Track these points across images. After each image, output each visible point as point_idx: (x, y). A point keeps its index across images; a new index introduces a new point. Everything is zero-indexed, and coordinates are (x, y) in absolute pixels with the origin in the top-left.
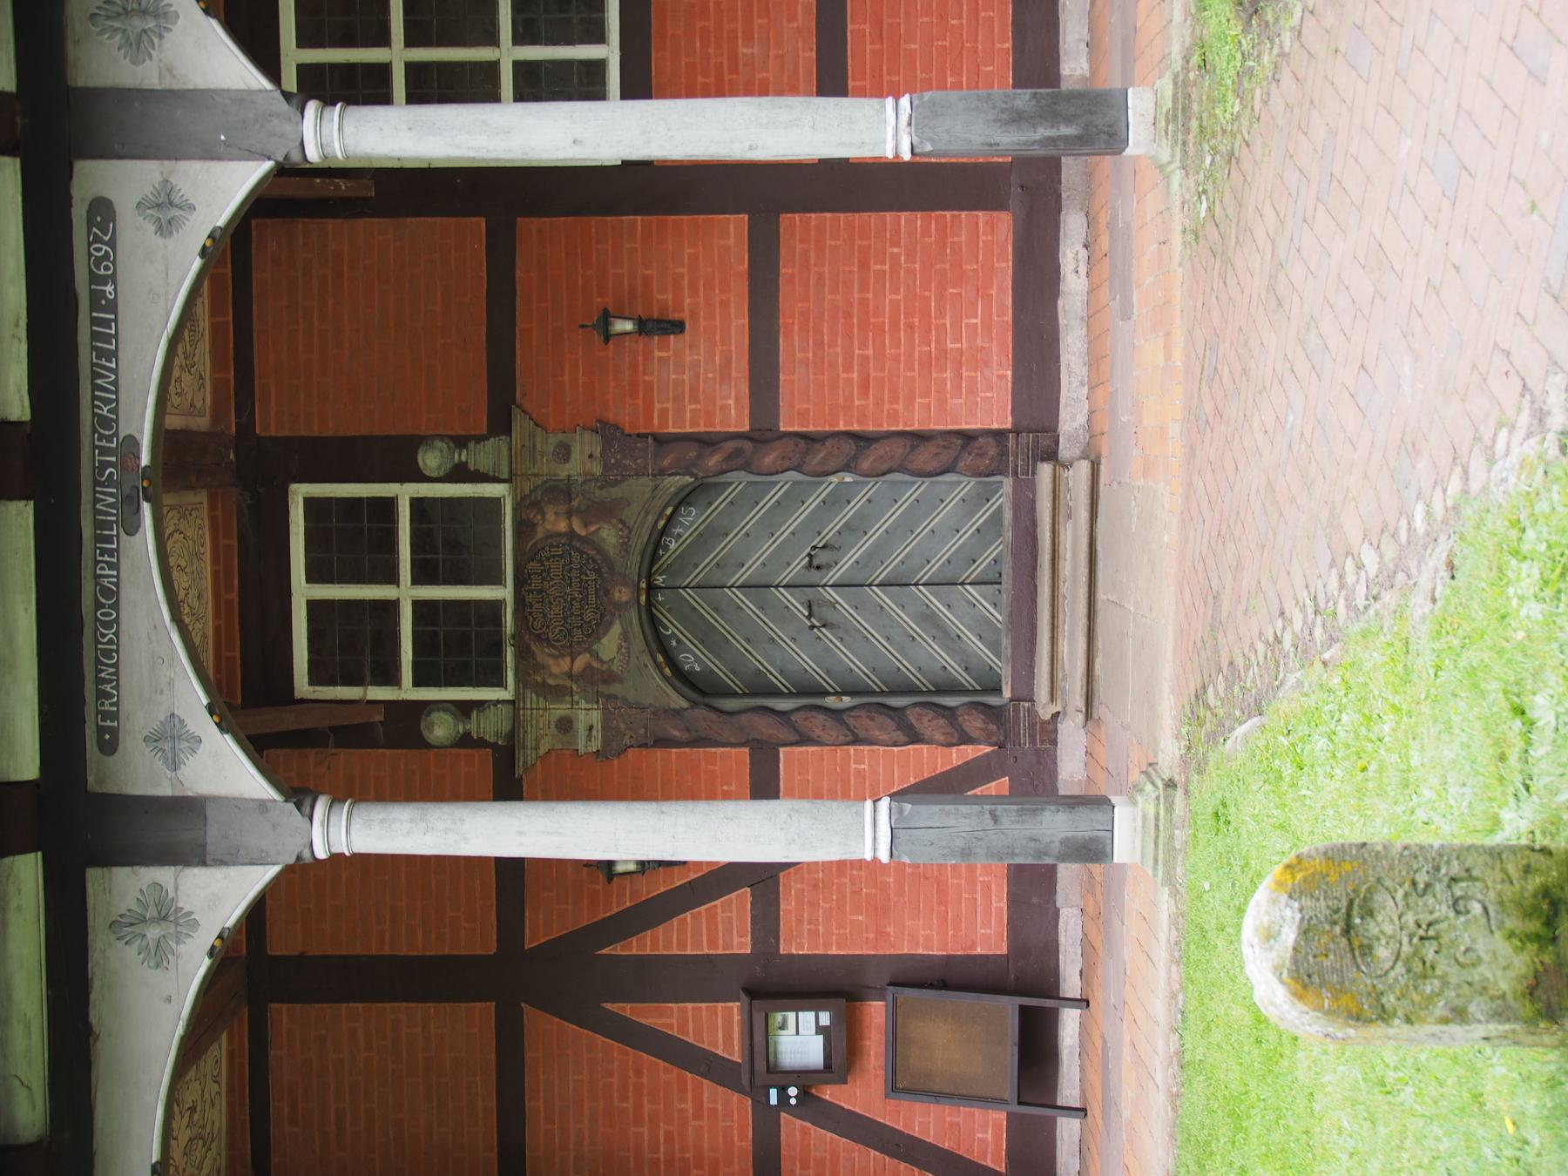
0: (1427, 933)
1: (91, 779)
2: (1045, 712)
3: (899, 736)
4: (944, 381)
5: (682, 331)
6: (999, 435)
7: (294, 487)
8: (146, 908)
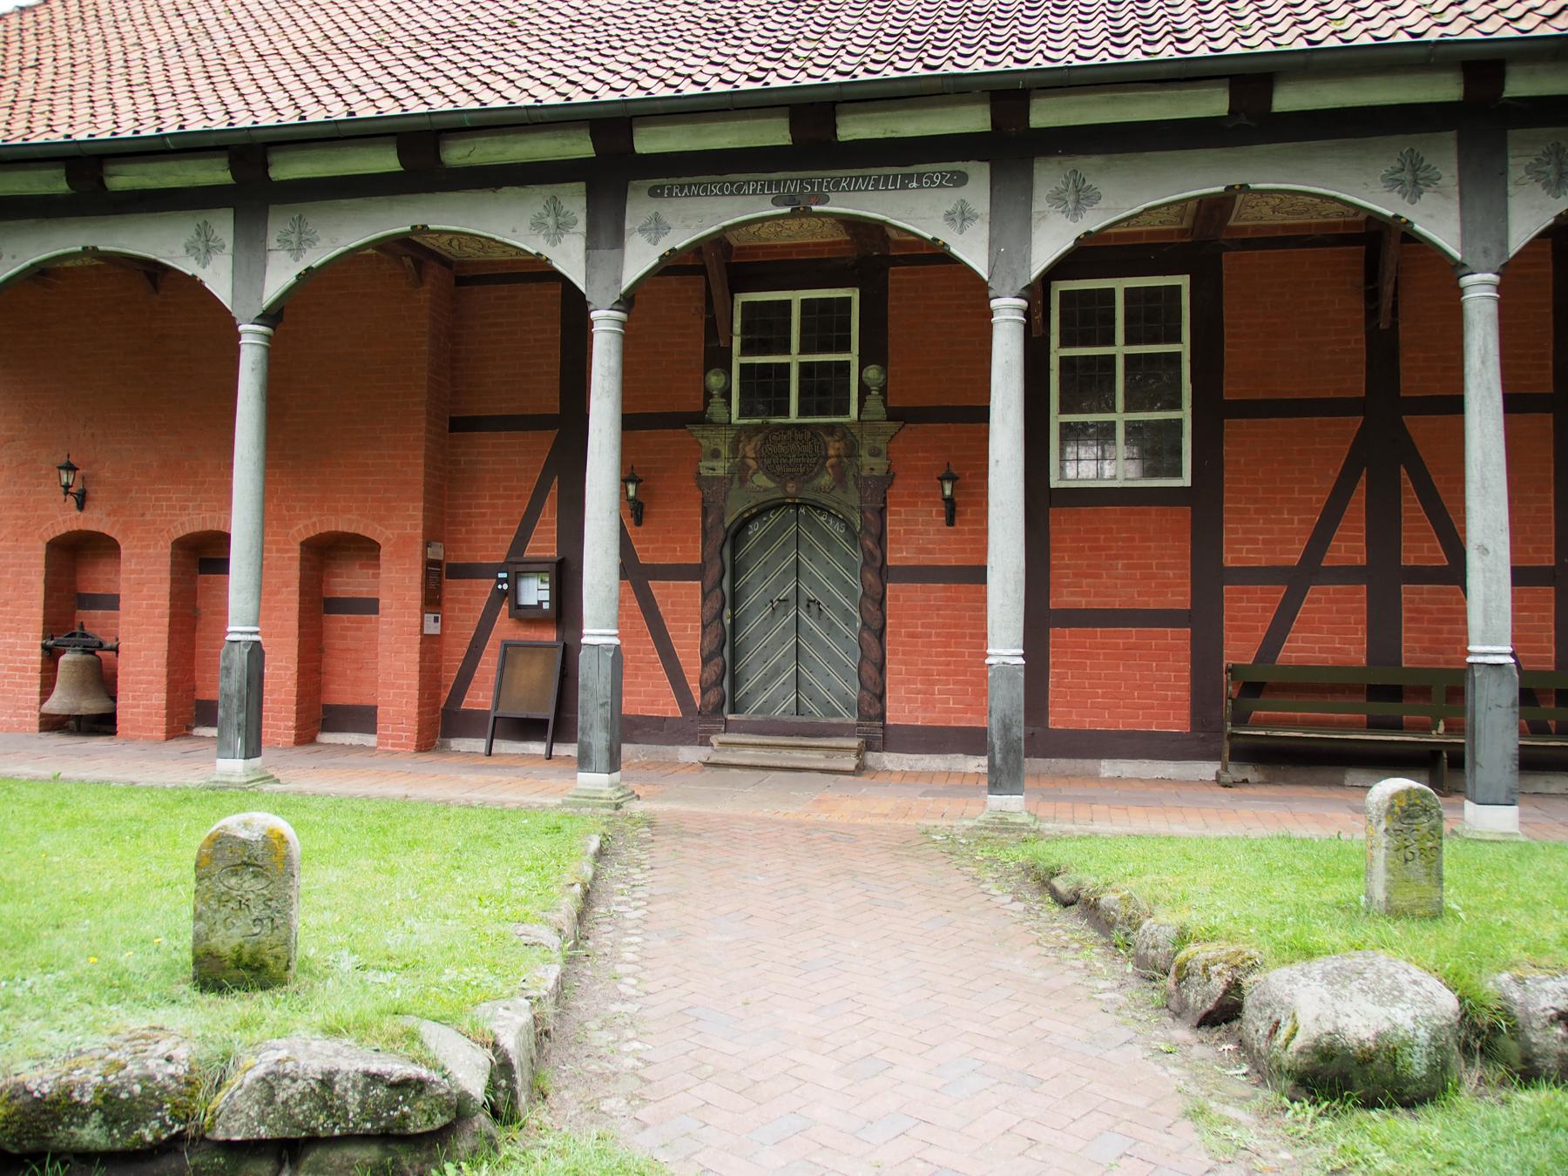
0: (243, 904)
1: (635, 182)
2: (714, 739)
3: (706, 652)
4: (916, 684)
5: (948, 525)
6: (882, 716)
7: (858, 290)
8: (564, 216)
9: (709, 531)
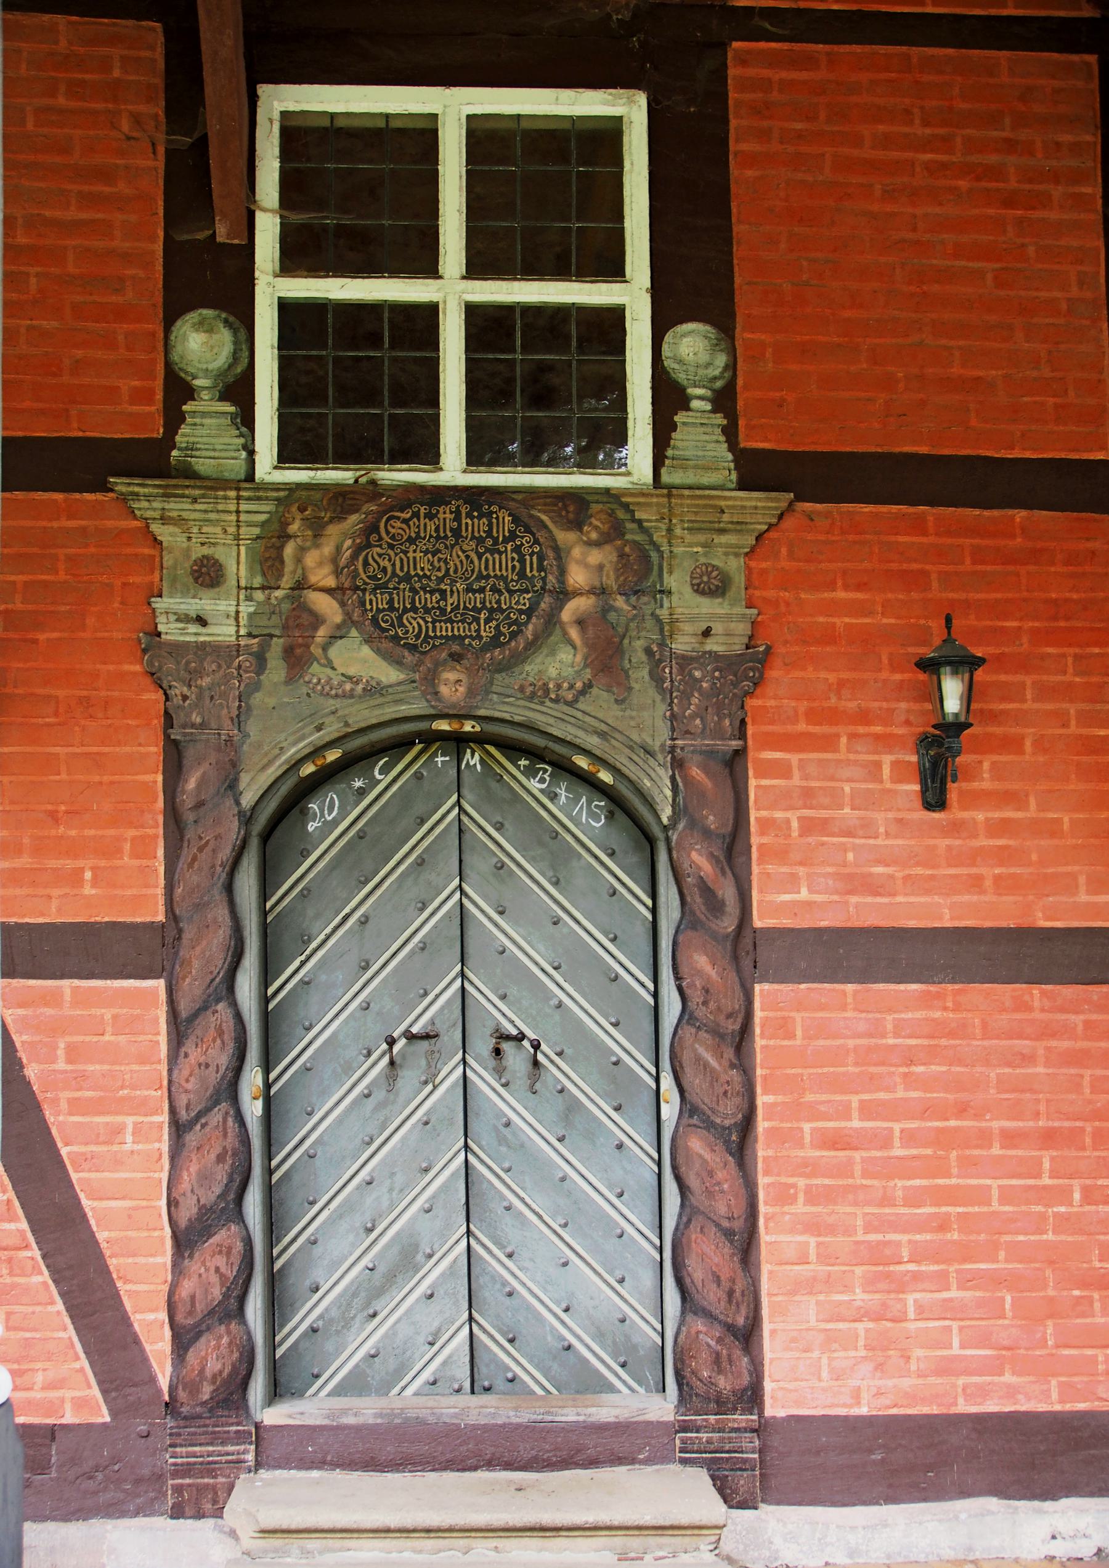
3: (187, 1212)
4: (848, 1288)
5: (929, 806)
6: (753, 1396)
7: (641, 99)
9: (190, 817)
